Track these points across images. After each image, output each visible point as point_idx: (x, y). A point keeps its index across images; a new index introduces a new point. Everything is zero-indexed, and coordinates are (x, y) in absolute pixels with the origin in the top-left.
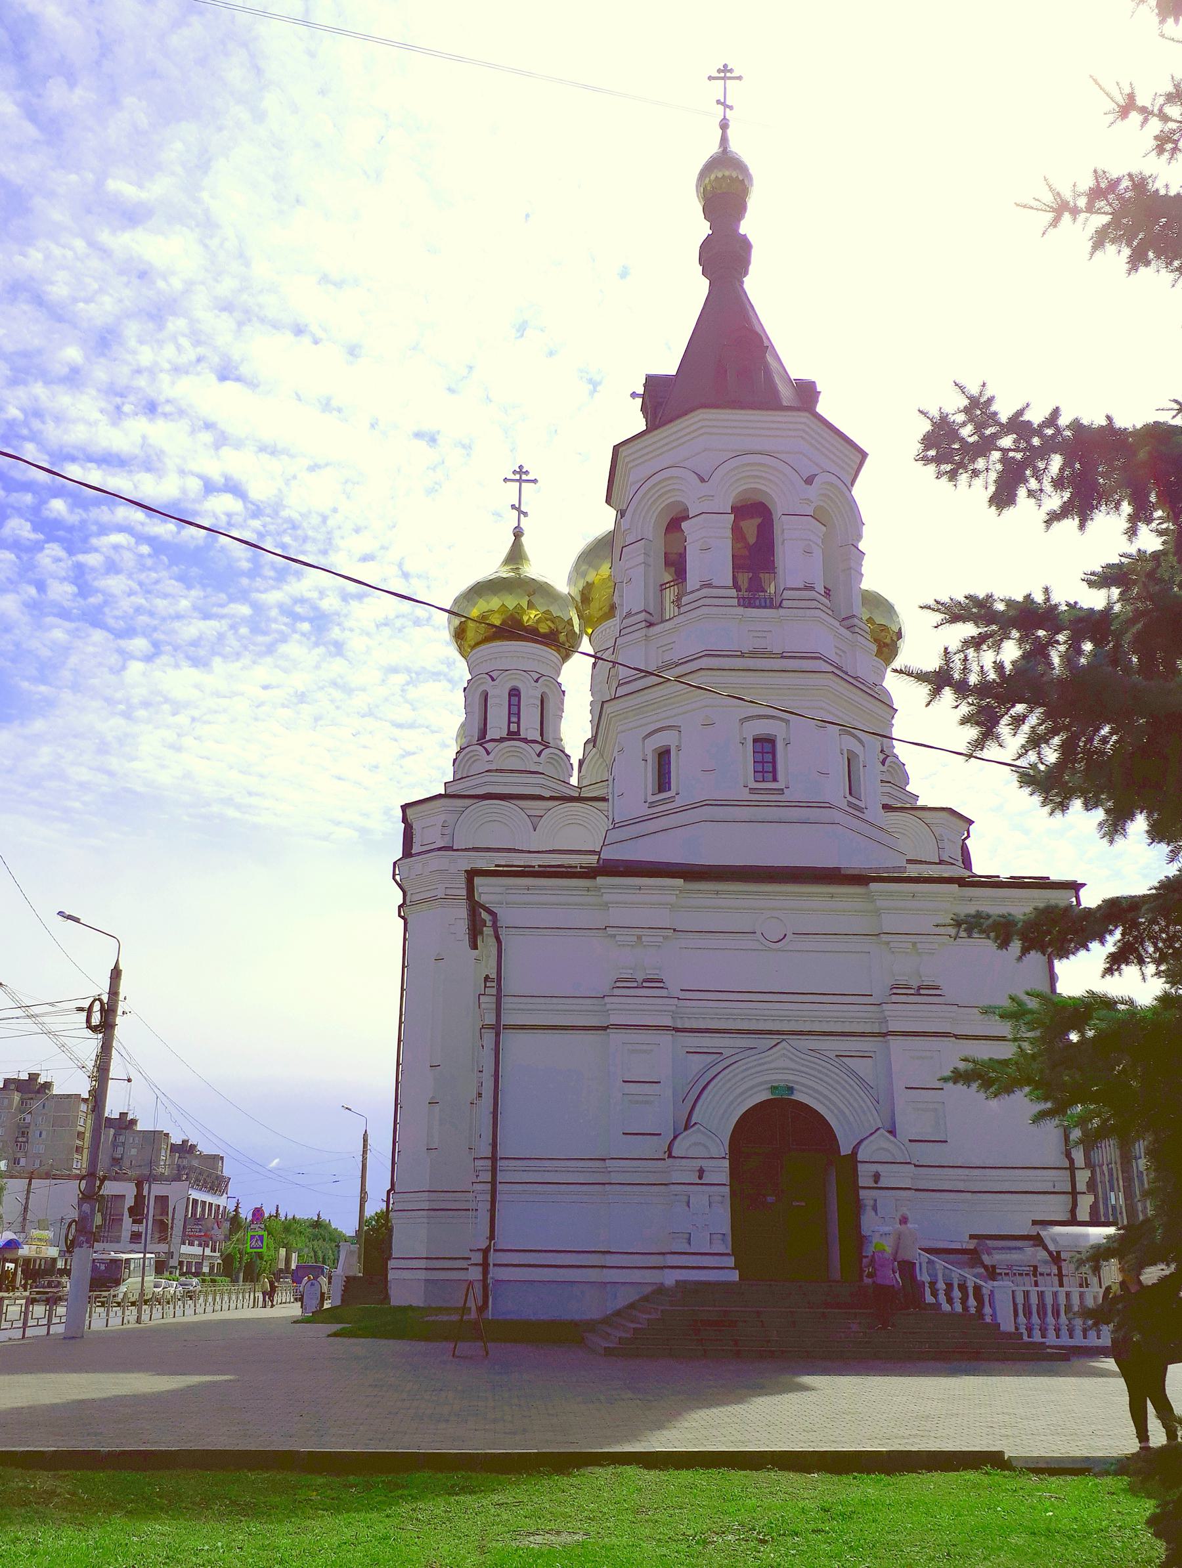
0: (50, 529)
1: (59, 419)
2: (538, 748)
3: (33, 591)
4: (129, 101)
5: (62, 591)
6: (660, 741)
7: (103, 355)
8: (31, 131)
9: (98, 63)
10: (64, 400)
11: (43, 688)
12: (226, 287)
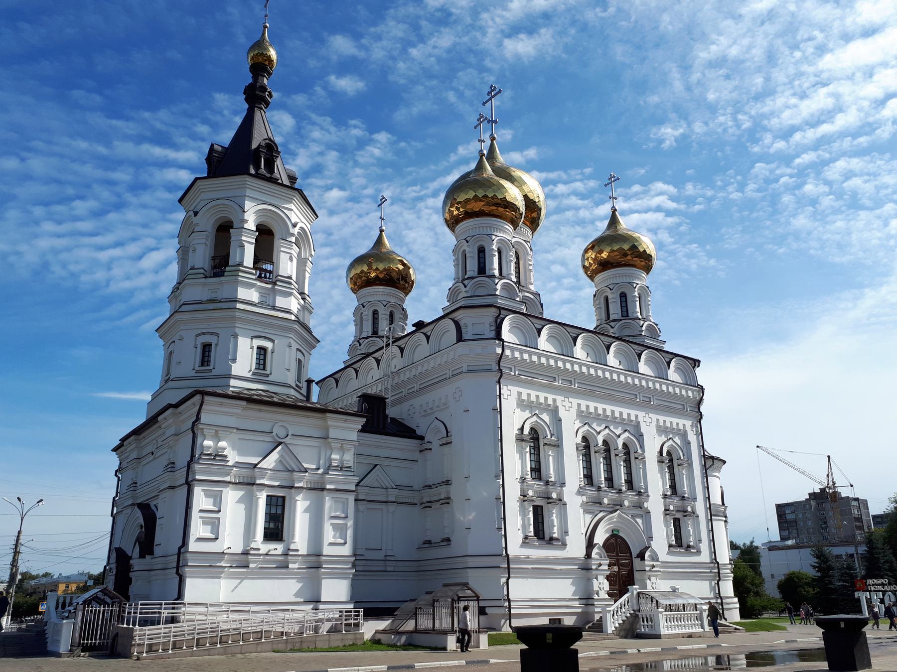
0: (802, 174)
1: (772, 114)
5: (827, 201)
10: (768, 106)
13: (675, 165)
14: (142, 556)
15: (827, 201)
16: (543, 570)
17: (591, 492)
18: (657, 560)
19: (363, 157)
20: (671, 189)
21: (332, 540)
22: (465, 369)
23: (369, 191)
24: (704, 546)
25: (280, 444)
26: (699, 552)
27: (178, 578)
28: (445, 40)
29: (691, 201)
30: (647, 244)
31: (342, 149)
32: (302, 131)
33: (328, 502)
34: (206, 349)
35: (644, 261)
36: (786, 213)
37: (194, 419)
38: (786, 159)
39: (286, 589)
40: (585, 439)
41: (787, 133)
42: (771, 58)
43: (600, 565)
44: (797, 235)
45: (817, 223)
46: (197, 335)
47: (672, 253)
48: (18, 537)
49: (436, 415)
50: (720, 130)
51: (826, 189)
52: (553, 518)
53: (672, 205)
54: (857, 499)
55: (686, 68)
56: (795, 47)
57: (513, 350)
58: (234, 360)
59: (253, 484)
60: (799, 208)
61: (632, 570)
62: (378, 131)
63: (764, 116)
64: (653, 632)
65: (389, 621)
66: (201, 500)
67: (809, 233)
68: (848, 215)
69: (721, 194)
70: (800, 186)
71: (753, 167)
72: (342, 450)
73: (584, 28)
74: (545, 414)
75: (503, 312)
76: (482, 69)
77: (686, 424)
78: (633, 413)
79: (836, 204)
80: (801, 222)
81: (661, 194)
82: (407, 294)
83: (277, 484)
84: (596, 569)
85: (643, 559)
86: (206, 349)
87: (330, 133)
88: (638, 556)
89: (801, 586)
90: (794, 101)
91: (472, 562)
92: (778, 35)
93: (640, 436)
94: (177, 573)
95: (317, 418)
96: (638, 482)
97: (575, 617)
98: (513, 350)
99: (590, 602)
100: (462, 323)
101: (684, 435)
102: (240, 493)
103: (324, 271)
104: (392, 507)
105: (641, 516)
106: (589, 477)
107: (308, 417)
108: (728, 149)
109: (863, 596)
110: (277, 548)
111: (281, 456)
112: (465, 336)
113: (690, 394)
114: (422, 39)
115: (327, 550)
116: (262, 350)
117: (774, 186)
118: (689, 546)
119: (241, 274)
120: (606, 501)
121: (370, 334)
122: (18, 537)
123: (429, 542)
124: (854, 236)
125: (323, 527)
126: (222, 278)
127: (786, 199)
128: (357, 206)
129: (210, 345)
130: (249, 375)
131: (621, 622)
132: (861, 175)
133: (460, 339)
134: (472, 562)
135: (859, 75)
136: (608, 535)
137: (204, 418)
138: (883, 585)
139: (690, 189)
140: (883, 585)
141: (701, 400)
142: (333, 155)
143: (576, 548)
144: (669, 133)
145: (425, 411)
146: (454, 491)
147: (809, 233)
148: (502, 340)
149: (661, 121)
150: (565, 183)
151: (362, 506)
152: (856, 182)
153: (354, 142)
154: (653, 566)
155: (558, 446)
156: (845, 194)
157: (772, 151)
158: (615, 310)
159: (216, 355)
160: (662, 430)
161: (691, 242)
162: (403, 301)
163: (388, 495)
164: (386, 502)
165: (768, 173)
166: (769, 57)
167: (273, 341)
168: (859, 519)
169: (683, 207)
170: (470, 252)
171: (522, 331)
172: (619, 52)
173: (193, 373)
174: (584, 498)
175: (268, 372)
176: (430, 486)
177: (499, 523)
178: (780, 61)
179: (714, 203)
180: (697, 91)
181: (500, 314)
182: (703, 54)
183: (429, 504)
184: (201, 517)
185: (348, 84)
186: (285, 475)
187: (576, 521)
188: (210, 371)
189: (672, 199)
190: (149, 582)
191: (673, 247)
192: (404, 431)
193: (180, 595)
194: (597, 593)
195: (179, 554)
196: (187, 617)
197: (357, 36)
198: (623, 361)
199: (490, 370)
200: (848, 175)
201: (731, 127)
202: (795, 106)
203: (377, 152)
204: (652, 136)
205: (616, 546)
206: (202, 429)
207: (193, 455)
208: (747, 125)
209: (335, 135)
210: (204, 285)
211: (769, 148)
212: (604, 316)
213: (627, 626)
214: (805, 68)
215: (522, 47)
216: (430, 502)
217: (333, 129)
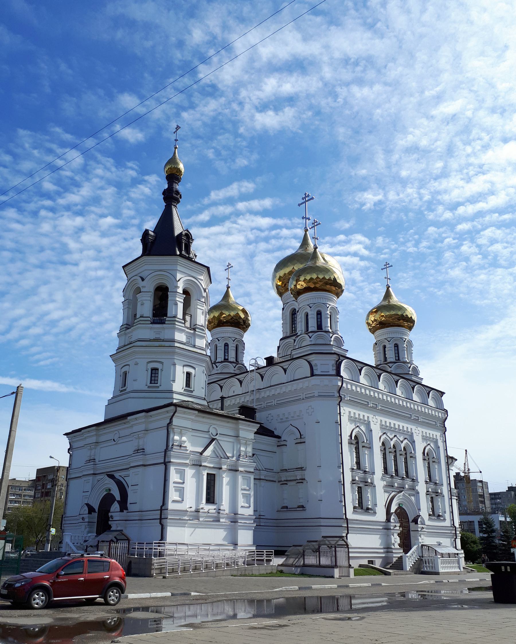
0: (461, 237)
1: (446, 191)
2: (234, 365)
3: (464, 263)
4: (418, 54)
5: (476, 259)
6: (124, 370)
7: (452, 156)
8: (388, 89)
9: (400, 47)
10: (444, 184)
11: (486, 301)
12: (489, 103)
13: (370, 222)
14: (121, 511)
15: (476, 259)
16: (365, 529)
18: (424, 524)
19: (136, 193)
20: (367, 241)
21: (243, 504)
22: (316, 395)
23: (136, 222)
24: (447, 516)
25: (213, 440)
26: (445, 520)
28: (210, 107)
29: (379, 250)
30: (341, 277)
31: (119, 185)
32: (88, 167)
33: (240, 478)
34: (154, 371)
35: (407, 322)
36: (447, 266)
37: (168, 422)
38: (451, 225)
39: (217, 535)
40: (383, 444)
41: (454, 207)
42: (450, 151)
43: (396, 526)
44: (452, 282)
45: (467, 275)
47: (361, 289)
50: (407, 200)
51: (477, 250)
53: (365, 252)
54: (481, 482)
55: (388, 152)
56: (468, 143)
57: (347, 383)
58: (174, 381)
59: (201, 466)
60: (455, 263)
61: (409, 531)
62: (148, 174)
63: (438, 193)
64: (433, 570)
65: (285, 559)
66: (174, 476)
67: (461, 282)
68: (489, 271)
69: (402, 248)
70: (458, 246)
71: (426, 230)
72: (246, 445)
73: (318, 113)
74: (362, 426)
75: (341, 358)
76: (236, 135)
77: (437, 434)
78: (410, 427)
79: (482, 262)
80: (456, 273)
81: (360, 243)
82: (245, 332)
83: (212, 466)
84: (393, 529)
85: (416, 523)
86: (154, 371)
87: (111, 172)
88: (413, 521)
89: (468, 543)
90: (461, 183)
91: (323, 522)
92: (457, 134)
93: (413, 442)
94: (160, 523)
95: (232, 423)
96: (412, 473)
97: (381, 560)
98: (347, 383)
99: (390, 550)
100: (313, 363)
101: (436, 442)
102: (193, 471)
103: (91, 280)
105: (413, 495)
107: (228, 422)
108: (411, 214)
110: (211, 508)
111: (215, 447)
112: (316, 372)
113: (440, 415)
114: (192, 106)
115: (241, 511)
116: (188, 374)
117: (440, 245)
118: (439, 516)
119: (176, 323)
120: (396, 485)
121: (223, 360)
123: (287, 507)
124: (492, 286)
125: (238, 495)
126: (164, 325)
127: (448, 255)
128: (124, 231)
129: (157, 369)
130: (182, 391)
131: (413, 563)
132: (502, 242)
133: (312, 375)
134: (323, 522)
135: (509, 169)
136: (397, 507)
137: (175, 421)
139: (380, 240)
141: (446, 418)
142: (111, 190)
143: (381, 515)
144: (370, 198)
145: (281, 419)
147: (461, 282)
148: (342, 377)
149: (364, 189)
150: (288, 228)
151: (257, 482)
152: (497, 247)
153: (129, 180)
154: (423, 528)
155: (370, 448)
156: (489, 255)
157: (442, 219)
158: (391, 356)
159: (162, 377)
160: (425, 438)
161: (375, 282)
162: (242, 336)
163: (260, 475)
164: (260, 479)
165: (437, 236)
166: (448, 150)
167: (194, 368)
168: (482, 496)
169: (372, 255)
170: (312, 314)
171: (350, 370)
172: (342, 132)
173: (146, 388)
174: (385, 483)
175: (192, 389)
176: (286, 470)
177: (341, 499)
178: (456, 154)
179: (395, 254)
180: (394, 170)
181: (339, 359)
182: (402, 142)
183: (285, 482)
184: (174, 487)
185: (131, 135)
186: (217, 460)
187: (381, 497)
188: (158, 387)
189: (366, 248)
191: (361, 284)
193: (163, 537)
194: (394, 545)
195: (161, 510)
196: (169, 552)
197: (142, 98)
198: (387, 386)
199: (333, 396)
200: (493, 241)
201: (415, 199)
202: (463, 187)
203: (147, 190)
204: (357, 199)
205: (401, 513)
208: (427, 197)
209: (114, 174)
210: (151, 328)
211: (440, 217)
212: (382, 359)
213: (416, 566)
214: (472, 160)
215: (269, 120)
216: (287, 481)
217: (114, 169)
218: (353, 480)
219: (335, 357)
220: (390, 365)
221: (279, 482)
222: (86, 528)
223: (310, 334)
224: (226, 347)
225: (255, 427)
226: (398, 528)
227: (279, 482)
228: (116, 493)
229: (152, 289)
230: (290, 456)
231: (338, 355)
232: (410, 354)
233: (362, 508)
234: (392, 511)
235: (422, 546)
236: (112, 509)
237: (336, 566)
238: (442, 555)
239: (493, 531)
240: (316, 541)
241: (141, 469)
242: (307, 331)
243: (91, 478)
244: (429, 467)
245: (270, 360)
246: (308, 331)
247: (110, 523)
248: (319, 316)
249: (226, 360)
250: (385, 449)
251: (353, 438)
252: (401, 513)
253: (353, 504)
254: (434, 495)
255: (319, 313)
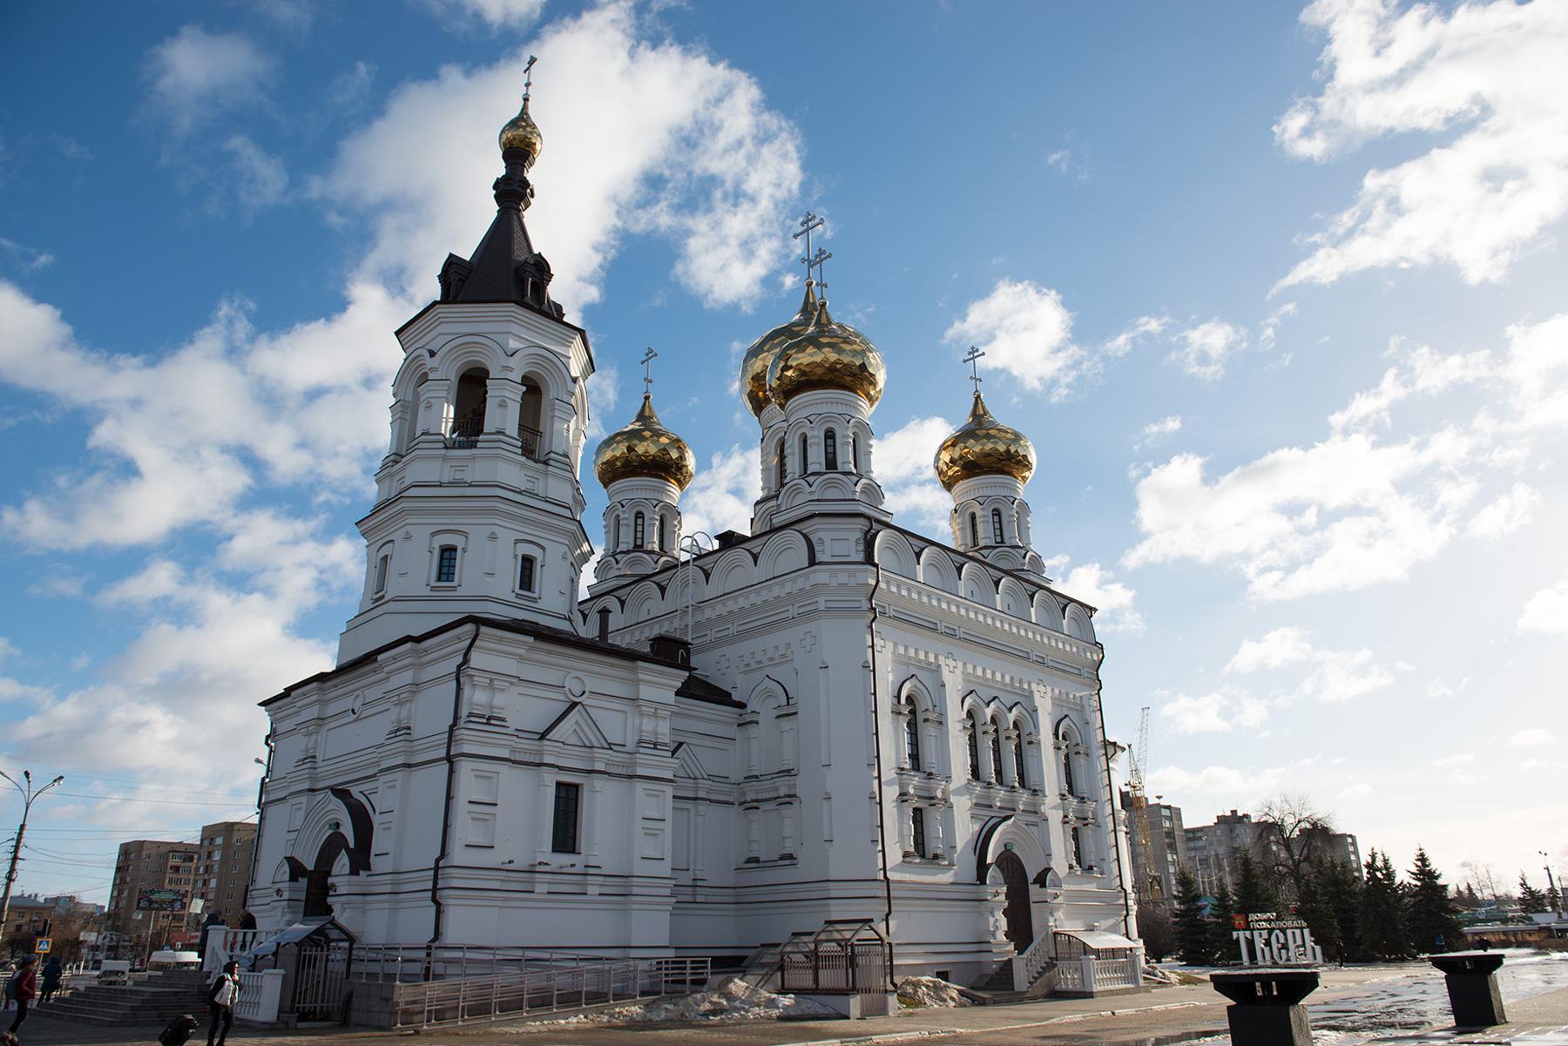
14: (354, 871)
17: (978, 788)
25: (574, 705)
27: (434, 908)
34: (448, 553)
40: (970, 714)
46: (434, 534)
48: (20, 834)
49: (768, 671)
52: (935, 831)
85: (1043, 885)
86: (448, 553)
88: (1035, 881)
94: (434, 899)
95: (623, 667)
96: (1032, 778)
100: (813, 538)
104: (703, 808)
106: (976, 772)
109: (1241, 936)
112: (819, 557)
121: (631, 547)
122: (20, 834)
123: (756, 860)
126: (474, 451)
129: (453, 549)
133: (812, 561)
137: (476, 659)
138: (1269, 920)
140: (1269, 920)
146: (802, 786)
148: (876, 566)
158: (985, 535)
163: (697, 789)
168: (1170, 834)
173: (427, 592)
190: (364, 912)
192: (720, 697)
195: (437, 869)
206: (472, 676)
207: (456, 718)
212: (969, 541)
218: (901, 794)
219: (861, 524)
220: (984, 552)
221: (741, 804)
222: (283, 914)
223: (811, 479)
224: (640, 521)
225: (678, 678)
226: (1002, 897)
227: (741, 804)
228: (348, 831)
229: (454, 377)
230: (764, 746)
231: (869, 518)
232: (1023, 529)
233: (923, 856)
234: (989, 861)
235: (1056, 934)
236: (336, 870)
237: (852, 990)
238: (1097, 952)
239: (1197, 897)
240: (811, 934)
241: (399, 775)
242: (805, 473)
243: (304, 799)
244: (1067, 766)
245: (729, 540)
246: (818, 497)
247: (330, 900)
248: (830, 442)
249: (638, 547)
250: (973, 726)
251: (903, 701)
252: (1010, 864)
253: (902, 847)
254: (1079, 824)
255: (830, 435)
